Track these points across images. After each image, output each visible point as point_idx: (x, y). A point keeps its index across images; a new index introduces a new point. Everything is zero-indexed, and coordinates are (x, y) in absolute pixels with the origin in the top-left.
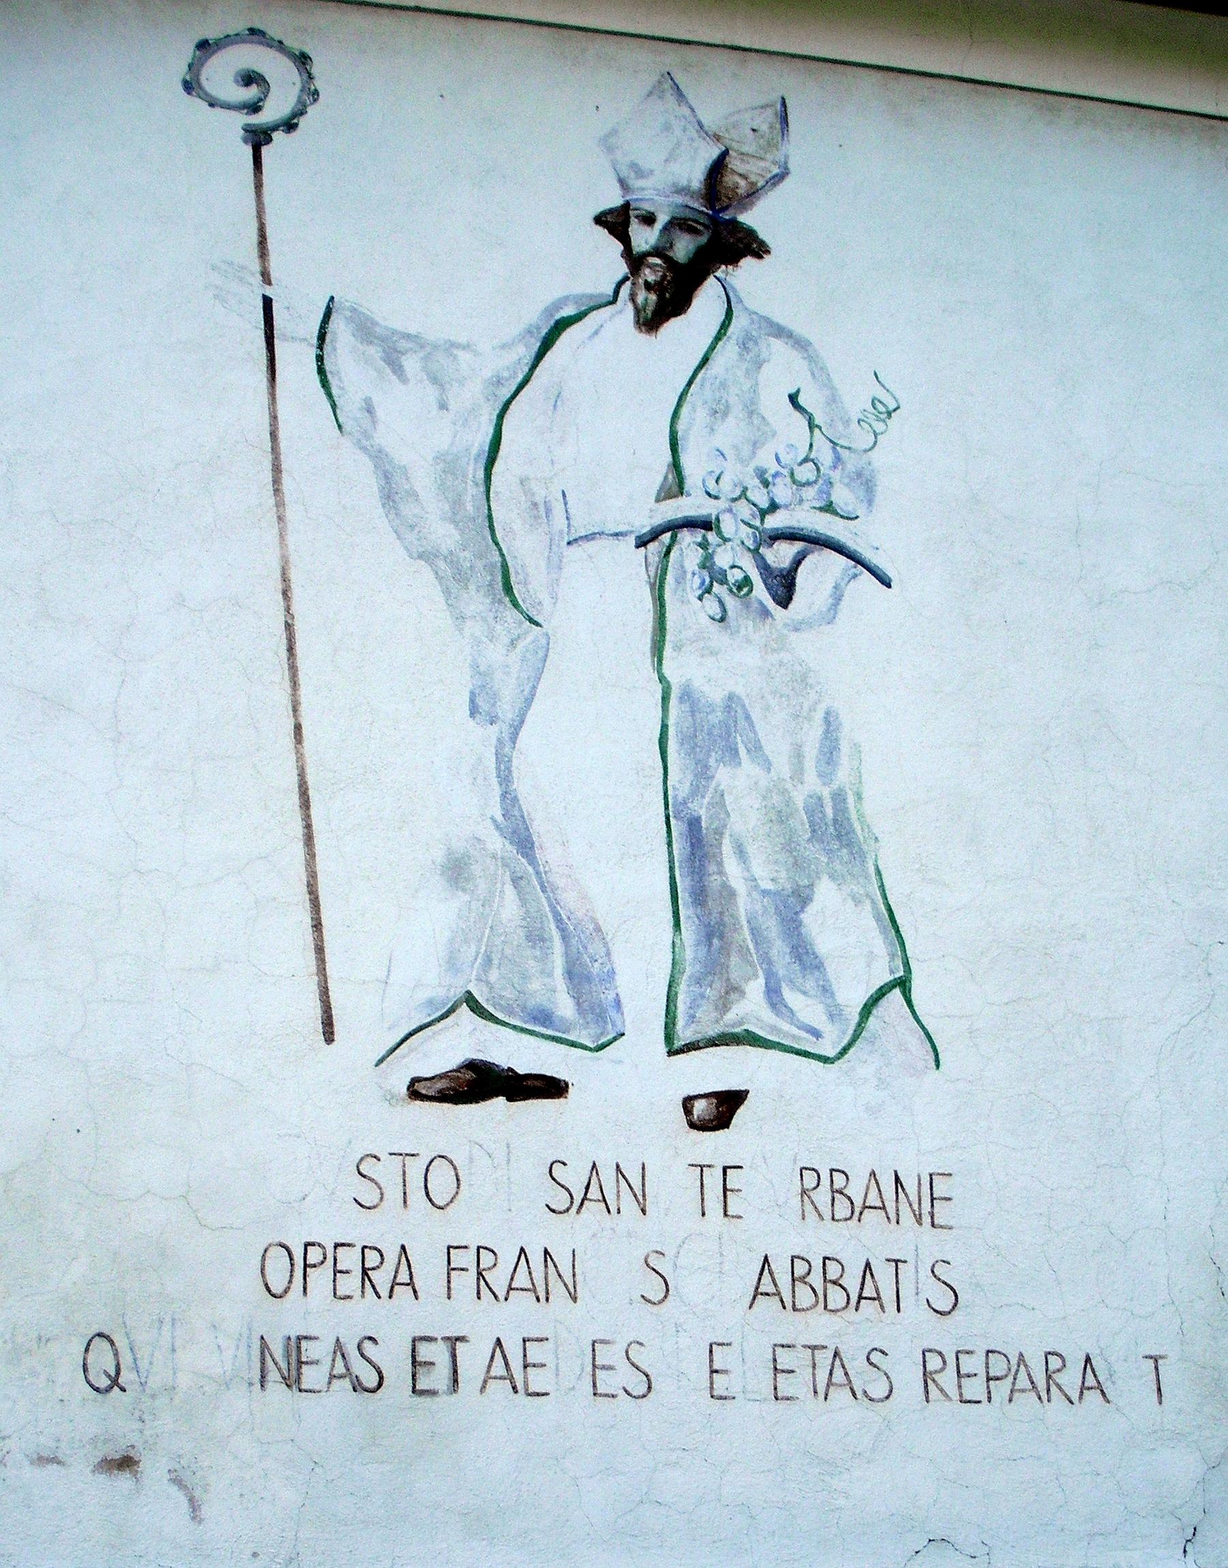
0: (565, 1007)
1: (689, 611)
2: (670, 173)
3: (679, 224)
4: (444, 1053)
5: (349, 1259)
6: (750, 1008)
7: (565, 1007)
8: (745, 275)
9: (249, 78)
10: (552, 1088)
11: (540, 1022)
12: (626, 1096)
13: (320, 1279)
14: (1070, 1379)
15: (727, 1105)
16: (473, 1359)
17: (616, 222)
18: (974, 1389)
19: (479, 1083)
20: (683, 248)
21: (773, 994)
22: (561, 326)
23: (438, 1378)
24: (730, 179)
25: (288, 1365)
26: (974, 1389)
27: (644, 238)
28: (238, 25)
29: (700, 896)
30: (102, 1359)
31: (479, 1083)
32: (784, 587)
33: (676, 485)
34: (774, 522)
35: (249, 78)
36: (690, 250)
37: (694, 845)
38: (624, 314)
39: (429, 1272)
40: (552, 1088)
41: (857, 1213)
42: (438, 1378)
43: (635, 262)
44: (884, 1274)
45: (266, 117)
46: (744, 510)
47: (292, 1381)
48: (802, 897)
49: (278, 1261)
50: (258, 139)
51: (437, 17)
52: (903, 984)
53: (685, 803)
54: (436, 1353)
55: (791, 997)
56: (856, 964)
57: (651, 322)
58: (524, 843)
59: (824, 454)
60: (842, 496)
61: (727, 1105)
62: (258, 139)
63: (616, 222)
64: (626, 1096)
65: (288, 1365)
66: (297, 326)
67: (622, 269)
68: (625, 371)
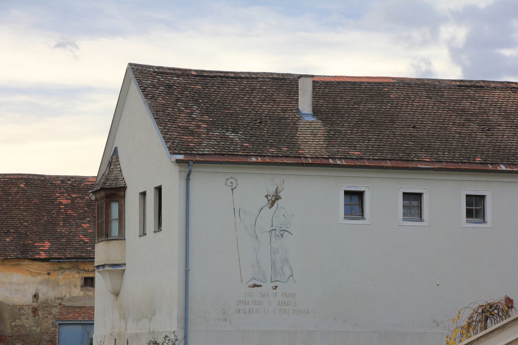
0: (262, 278)
1: (273, 239)
2: (272, 192)
3: (273, 196)
4: (251, 283)
5: (244, 302)
6: (278, 278)
7: (262, 278)
8: (279, 201)
9: (231, 183)
10: (261, 286)
11: (260, 280)
12: (267, 287)
13: (241, 303)
14: (306, 312)
15: (276, 287)
16: (254, 310)
17: (267, 196)
18: (297, 313)
19: (255, 286)
20: (273, 199)
21: (280, 276)
22: (262, 209)
23: (251, 312)
24: (278, 190)
25: (239, 311)
26: (297, 313)
27: (269, 198)
28: (230, 177)
29: (274, 268)
30: (223, 311)
31: (255, 286)
32: (282, 236)
33: (272, 226)
34: (282, 229)
35: (231, 183)
36: (274, 199)
37: (273, 262)
38: (268, 207)
39: (250, 302)
40: (261, 286)
41: (287, 297)
42: (251, 312)
43: (269, 201)
44: (290, 303)
45: (233, 187)
46: (279, 228)
47: (239, 313)
48: (283, 267)
49: (238, 302)
50: (232, 190)
51: (185, 287)
52: (292, 275)
53: (55, 317)
54: (251, 310)
55: (282, 277)
56: (288, 273)
57: (270, 208)
58: (258, 263)
59: (286, 221)
60: (288, 226)
61: (276, 287)
62: (232, 190)
63: (267, 196)
64: (267, 287)
65: (239, 311)
66: (237, 210)
67: (267, 202)
68: (268, 212)
